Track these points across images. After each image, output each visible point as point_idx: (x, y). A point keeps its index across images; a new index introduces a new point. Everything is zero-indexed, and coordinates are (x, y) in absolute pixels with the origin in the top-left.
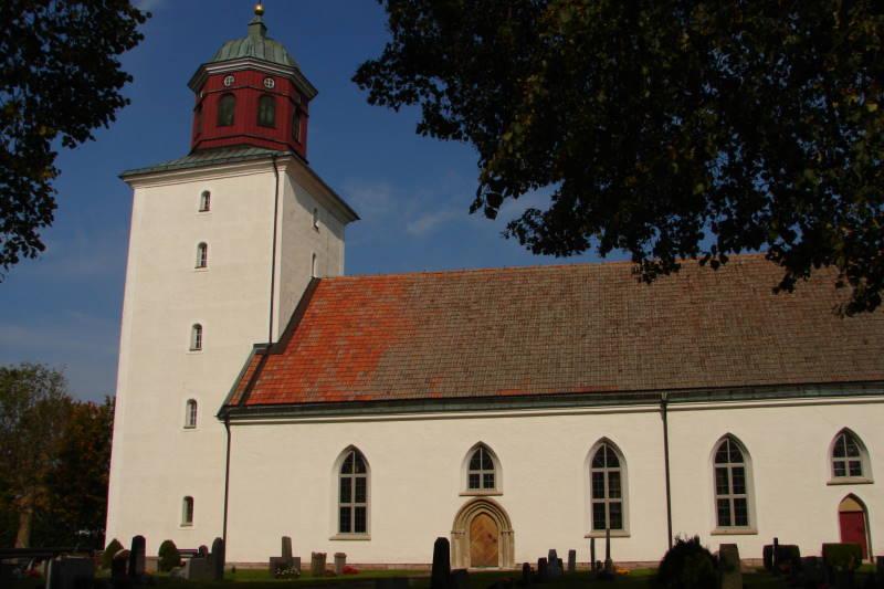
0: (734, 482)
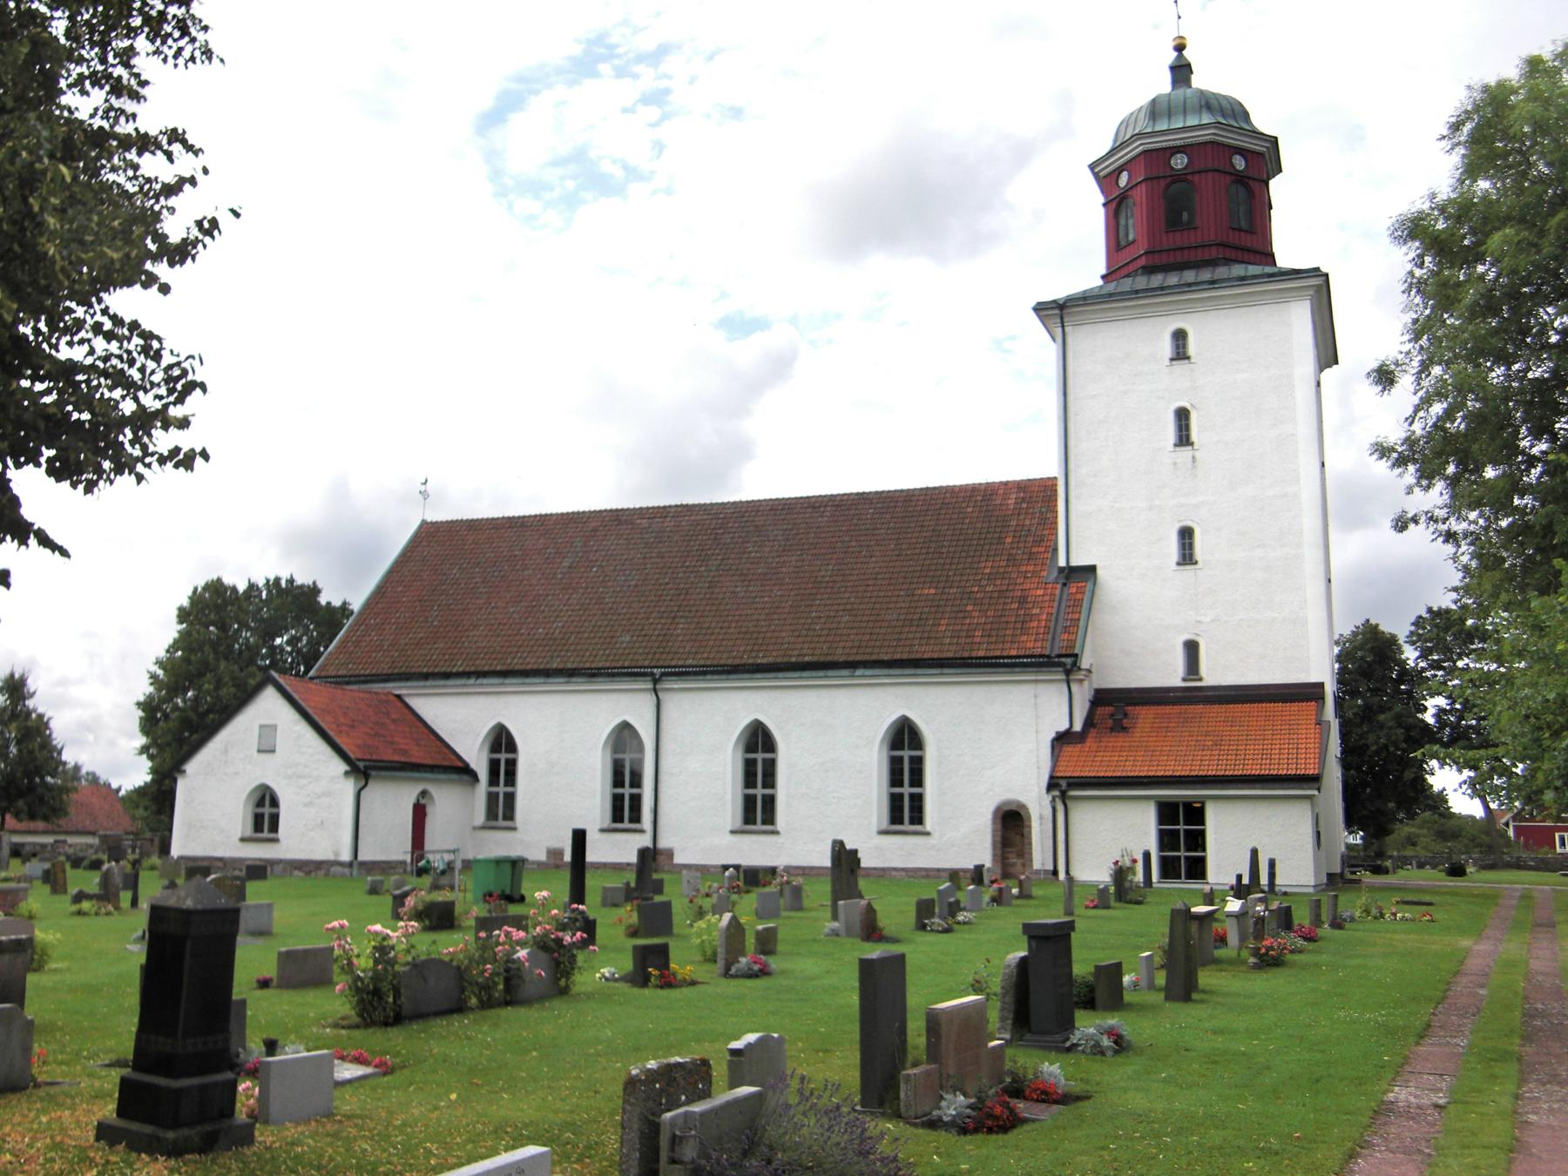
0: (902, 770)
